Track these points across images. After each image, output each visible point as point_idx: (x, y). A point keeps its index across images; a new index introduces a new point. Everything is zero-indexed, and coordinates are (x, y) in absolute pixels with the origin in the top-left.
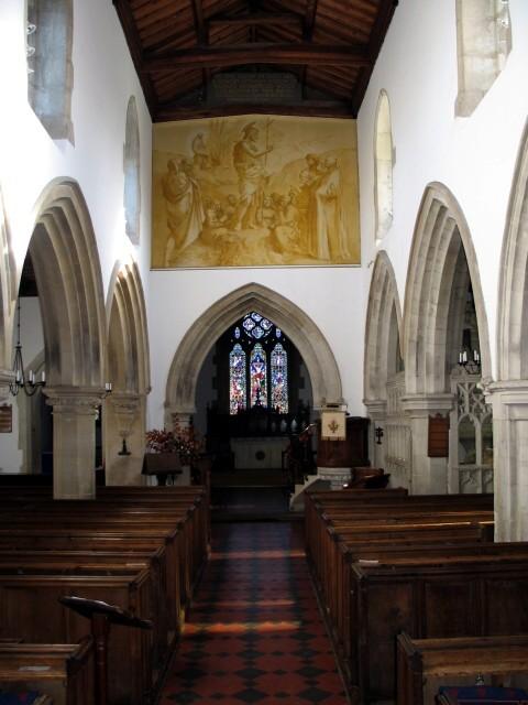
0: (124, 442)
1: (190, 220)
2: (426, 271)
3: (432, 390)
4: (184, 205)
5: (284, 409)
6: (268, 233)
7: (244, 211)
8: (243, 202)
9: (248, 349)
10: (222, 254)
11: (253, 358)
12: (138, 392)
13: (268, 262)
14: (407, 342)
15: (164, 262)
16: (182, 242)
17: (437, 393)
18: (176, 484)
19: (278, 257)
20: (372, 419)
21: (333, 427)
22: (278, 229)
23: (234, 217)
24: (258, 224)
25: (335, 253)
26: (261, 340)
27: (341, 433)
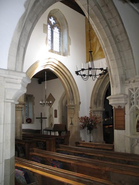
0: (72, 120)
1: (97, 44)
12: (74, 103)
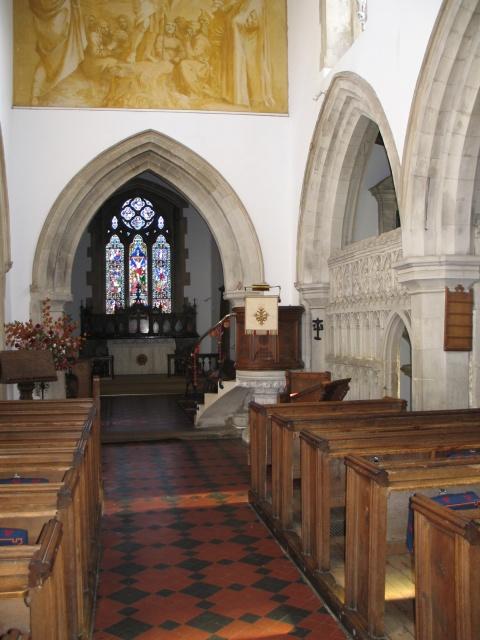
2: (458, 59)
3: (451, 249)
4: (59, 24)
5: (167, 309)
6: (170, 67)
7: (139, 37)
8: (138, 26)
9: (127, 241)
10: (111, 92)
11: (132, 251)
13: (170, 105)
14: (409, 179)
15: (31, 100)
16: (57, 73)
17: (458, 254)
18: (48, 396)
19: (184, 99)
20: (307, 308)
21: (261, 318)
22: (184, 64)
23: (126, 45)
24: (157, 55)
25: (257, 99)
26: (142, 232)
27: (272, 325)
